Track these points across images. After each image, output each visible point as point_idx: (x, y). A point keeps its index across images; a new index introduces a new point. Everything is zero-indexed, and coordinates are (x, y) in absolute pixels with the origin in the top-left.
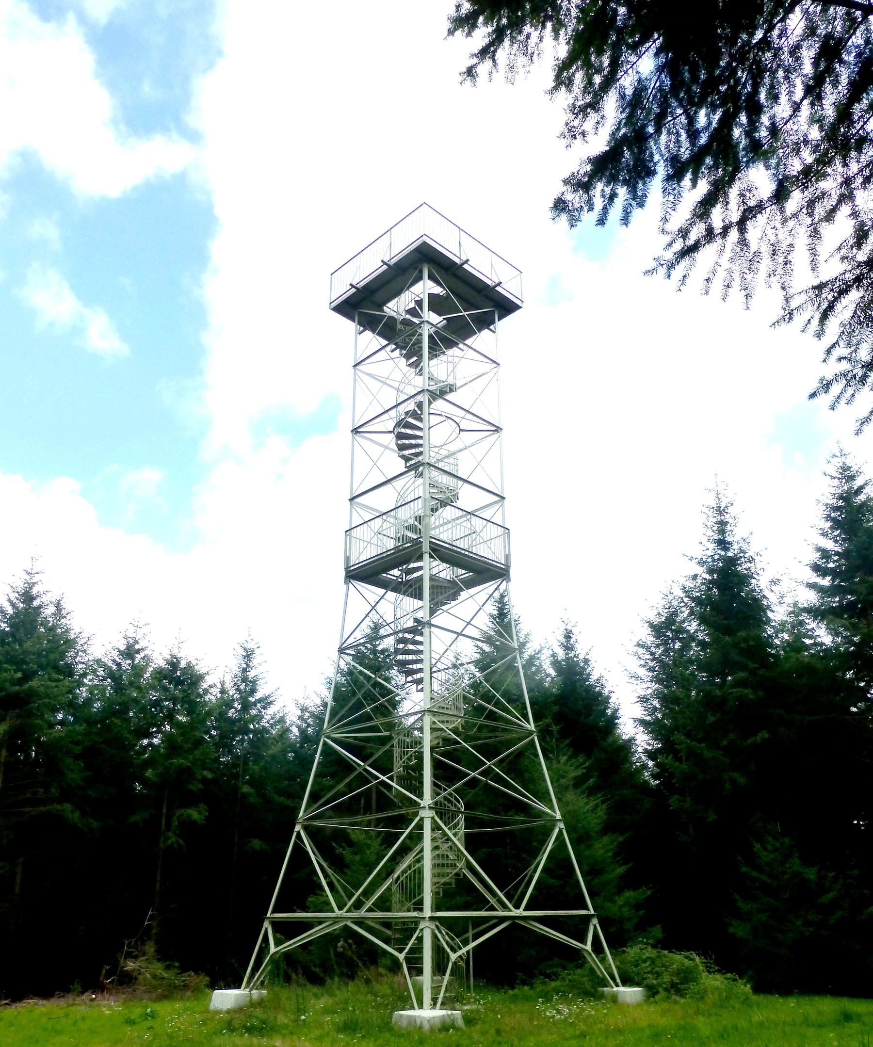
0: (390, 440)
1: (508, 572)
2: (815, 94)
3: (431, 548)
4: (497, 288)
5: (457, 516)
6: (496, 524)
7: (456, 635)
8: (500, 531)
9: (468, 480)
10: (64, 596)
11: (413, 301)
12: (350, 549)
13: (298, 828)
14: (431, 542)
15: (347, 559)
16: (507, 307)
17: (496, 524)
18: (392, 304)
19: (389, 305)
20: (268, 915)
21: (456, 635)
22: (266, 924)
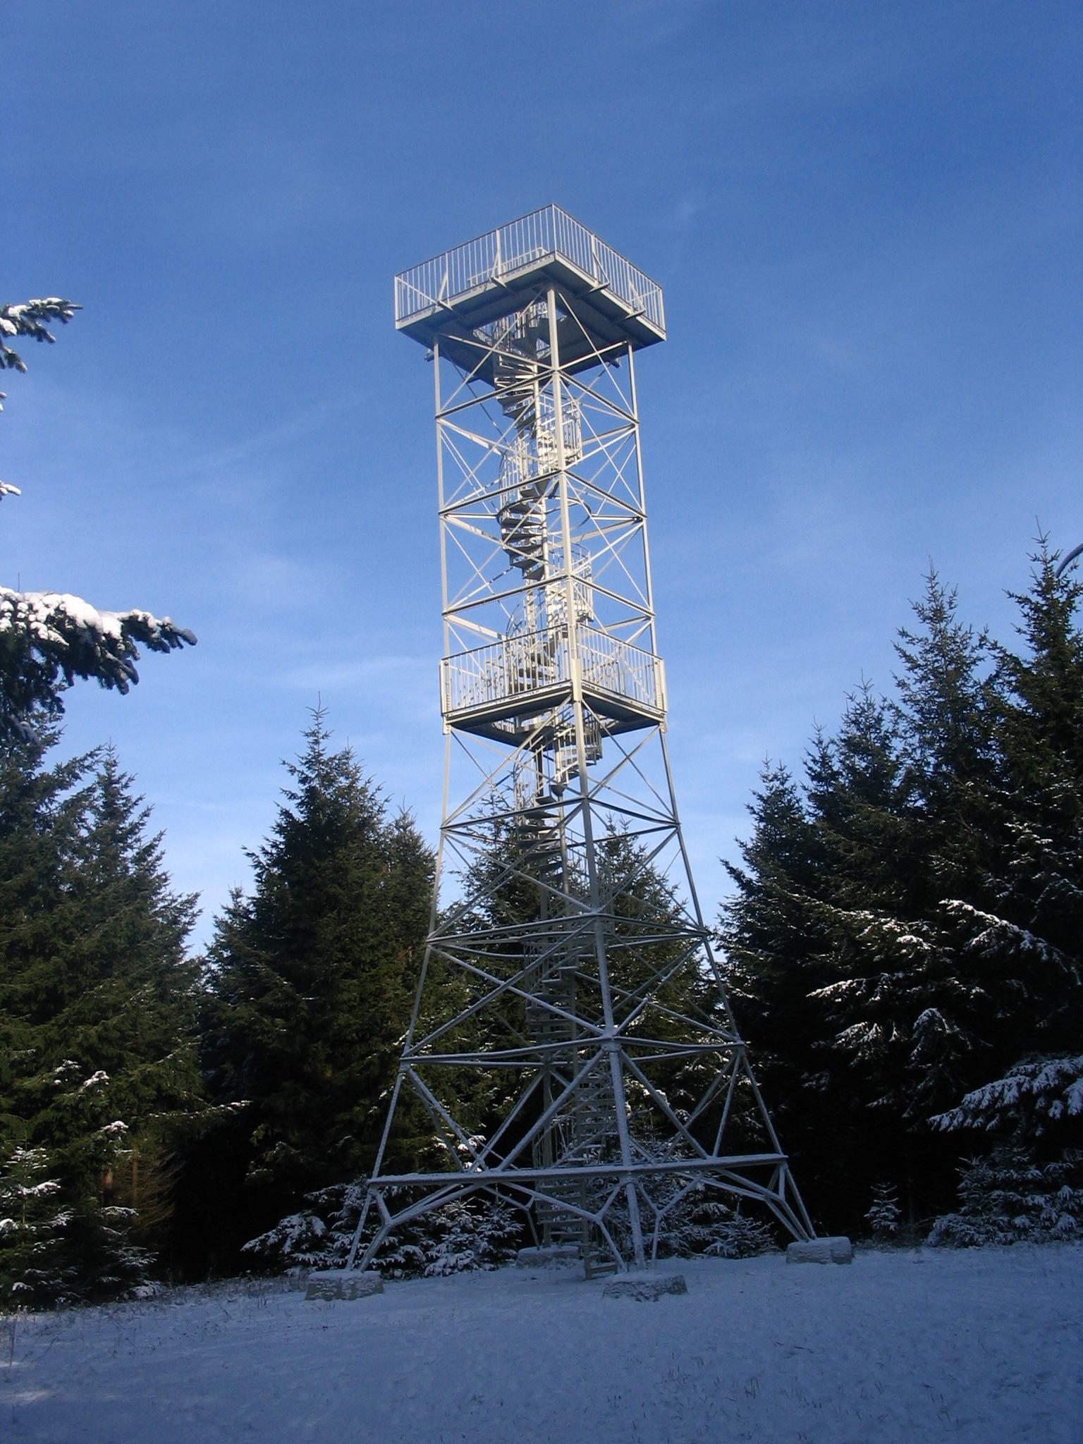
3: (585, 696)
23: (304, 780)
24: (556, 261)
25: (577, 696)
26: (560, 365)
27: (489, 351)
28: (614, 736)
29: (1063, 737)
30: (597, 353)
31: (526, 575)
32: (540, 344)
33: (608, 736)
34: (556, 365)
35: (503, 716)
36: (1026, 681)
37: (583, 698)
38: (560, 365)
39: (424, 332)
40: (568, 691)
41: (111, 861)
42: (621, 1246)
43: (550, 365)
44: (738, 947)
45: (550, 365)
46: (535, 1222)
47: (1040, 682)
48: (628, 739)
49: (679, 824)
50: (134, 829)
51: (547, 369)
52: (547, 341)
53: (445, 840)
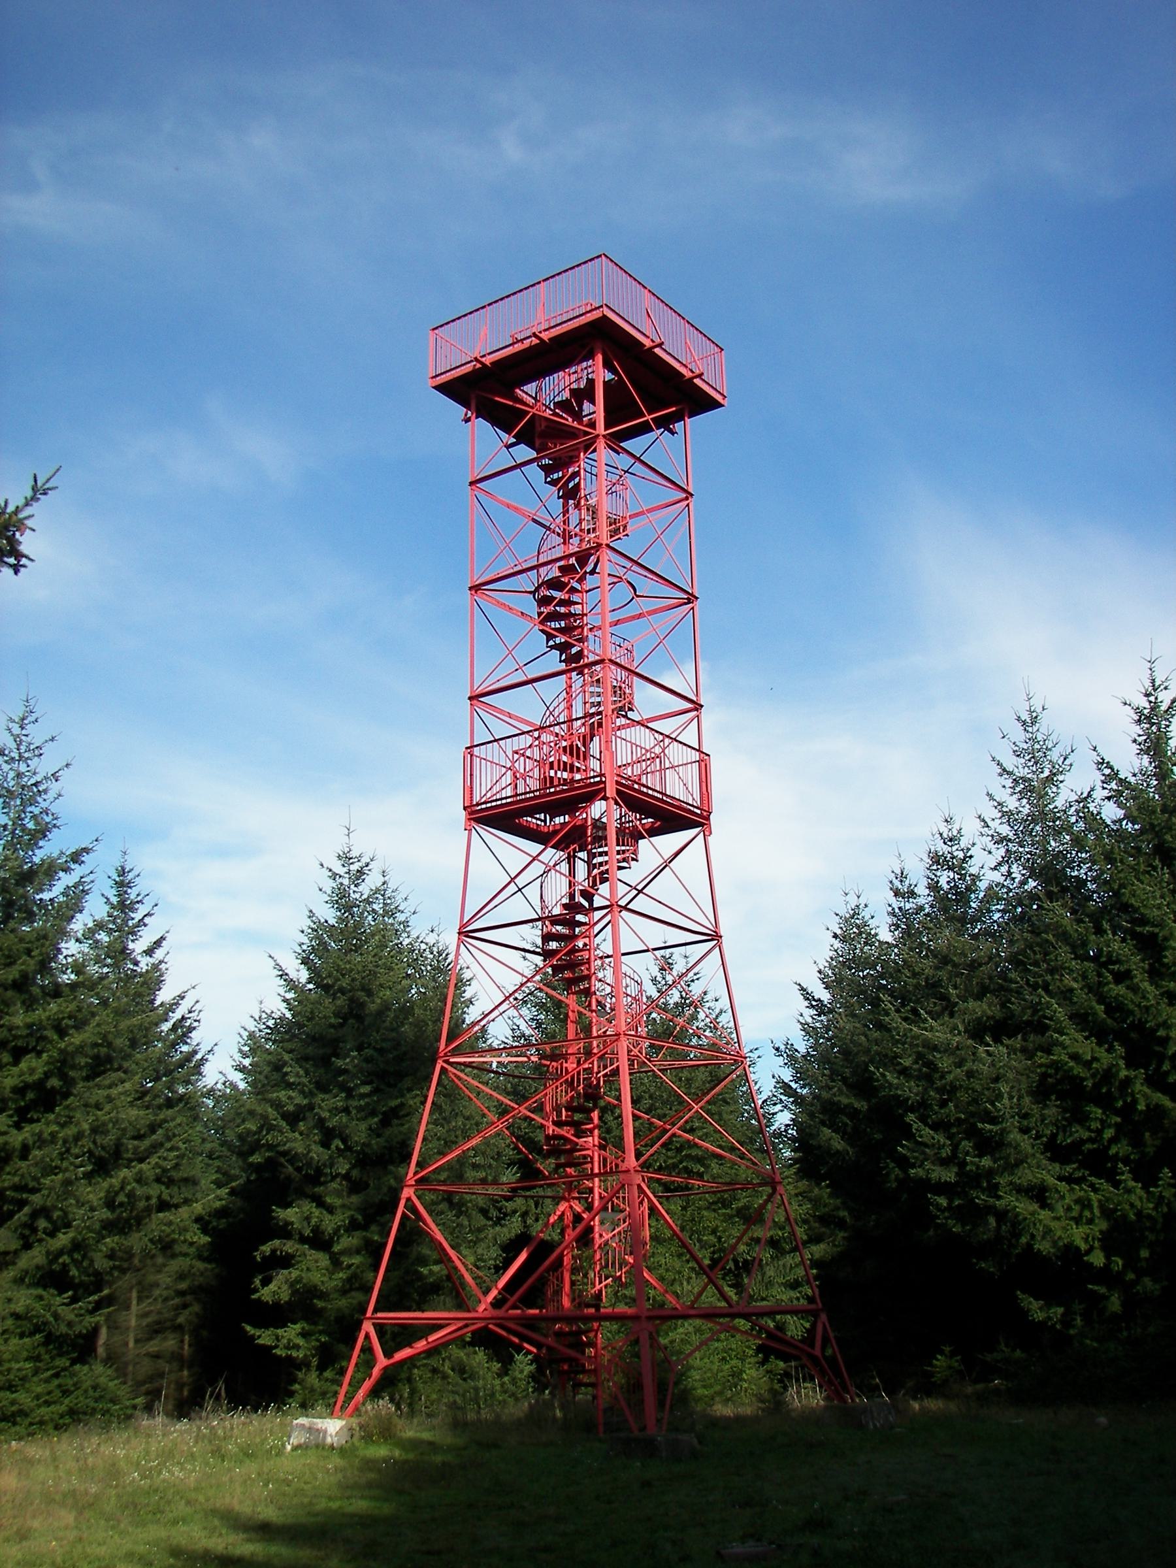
0: (531, 607)
1: (708, 819)
2: (1151, 1237)
3: (619, 792)
4: (695, 381)
5: (623, 731)
6: (685, 745)
7: (628, 907)
8: (695, 756)
9: (637, 670)
10: (98, 847)
11: (567, 389)
12: (471, 775)
13: (407, 1192)
14: (618, 783)
15: (469, 790)
16: (702, 403)
17: (685, 745)
18: (531, 388)
19: (525, 388)
20: (369, 1314)
21: (628, 907)
22: (368, 1327)
23: (334, 876)
24: (604, 316)
25: (611, 791)
26: (605, 430)
27: (529, 412)
28: (652, 839)
29: (1163, 852)
30: (649, 418)
31: (549, 479)
32: (587, 407)
33: (645, 838)
34: (601, 429)
35: (532, 811)
36: (1121, 789)
37: (617, 794)
38: (605, 430)
39: (456, 389)
40: (602, 786)
41: (119, 953)
42: (603, 1116)
43: (595, 429)
44: (852, 1146)
45: (595, 429)
46: (548, 1270)
47: (1136, 793)
48: (669, 842)
49: (721, 937)
50: (141, 923)
51: (592, 433)
52: (593, 402)
53: (462, 945)
